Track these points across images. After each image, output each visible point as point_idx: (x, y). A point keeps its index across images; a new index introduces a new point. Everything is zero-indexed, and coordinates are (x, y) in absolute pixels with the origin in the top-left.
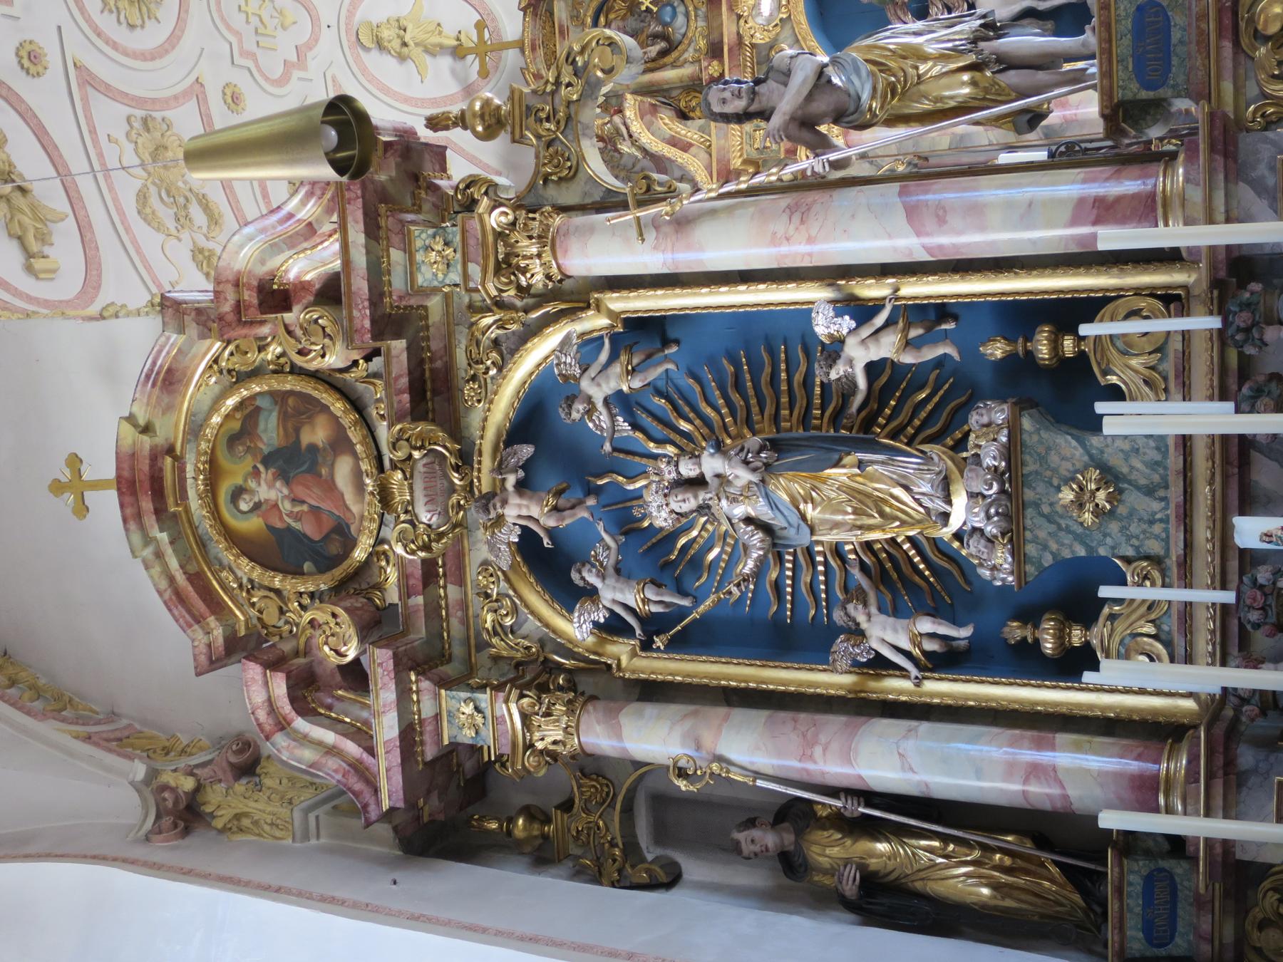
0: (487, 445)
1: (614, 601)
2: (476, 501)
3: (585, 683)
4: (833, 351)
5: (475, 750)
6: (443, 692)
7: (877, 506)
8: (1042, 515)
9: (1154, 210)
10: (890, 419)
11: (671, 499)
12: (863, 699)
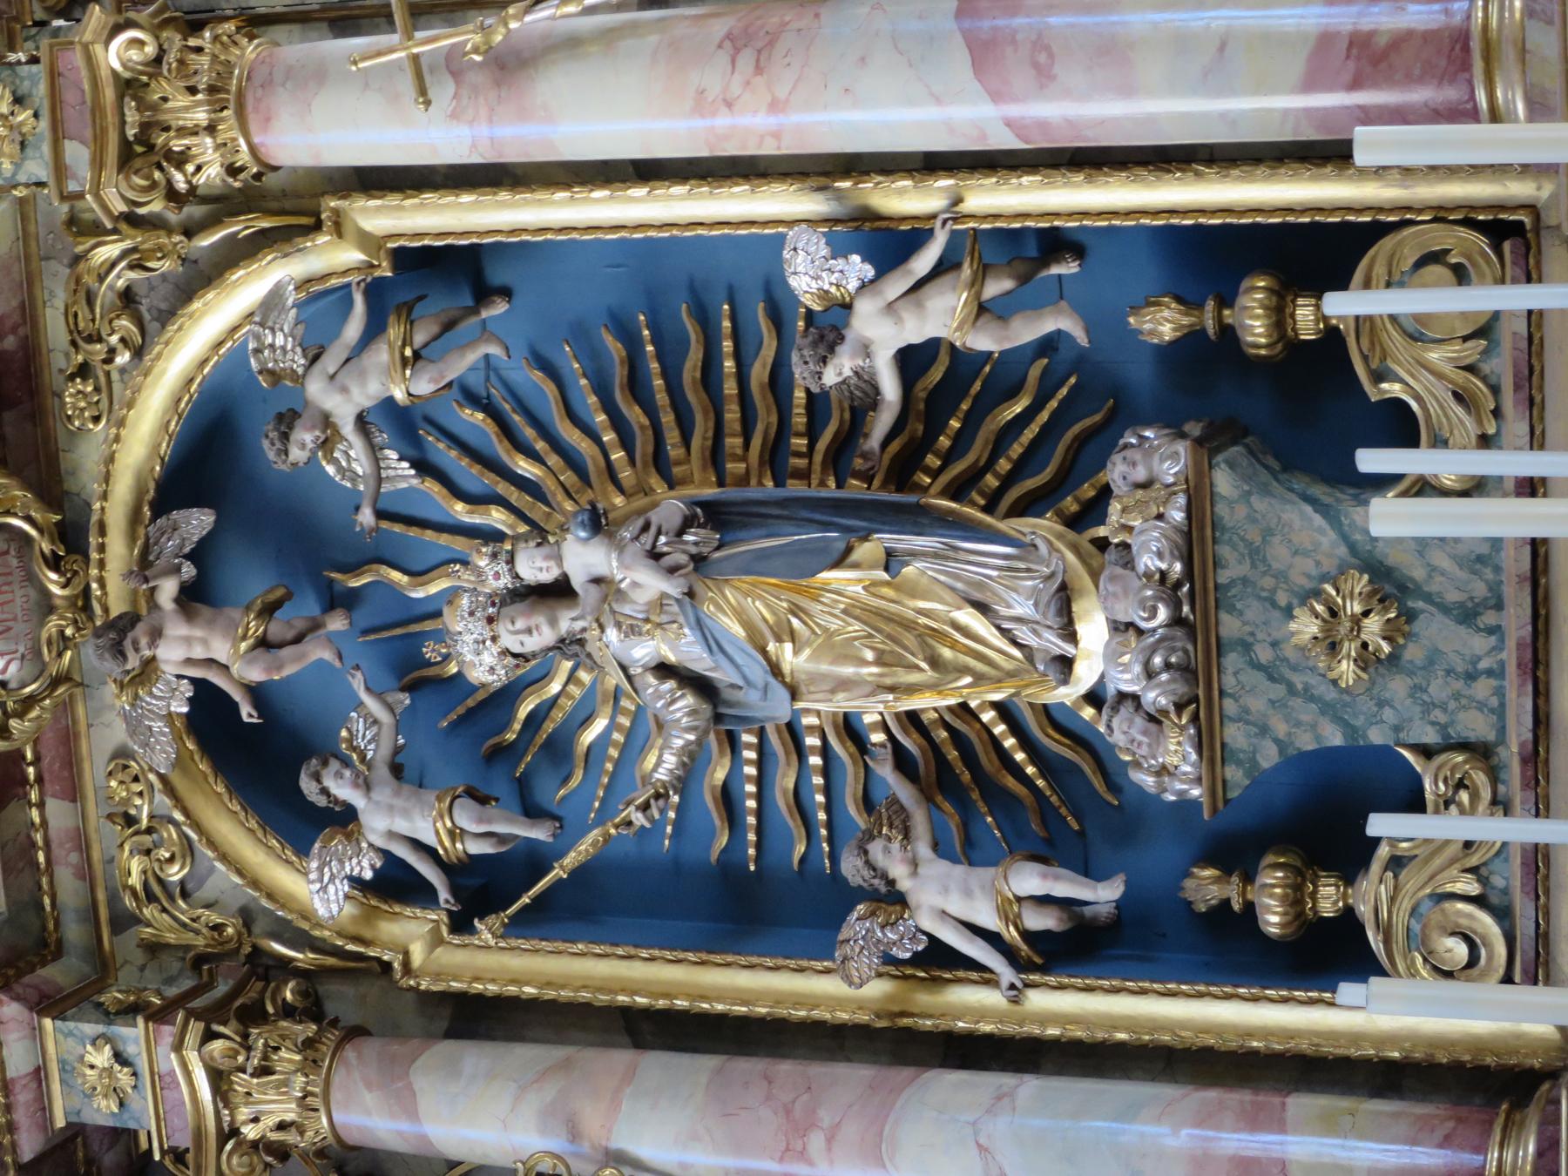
0: (116, 508)
1: (392, 835)
2: (98, 633)
3: (342, 1001)
4: (829, 325)
5: (122, 1136)
6: (48, 1023)
7: (924, 645)
8: (1257, 666)
9: (1466, 66)
10: (949, 458)
11: (503, 628)
12: (907, 1030)
